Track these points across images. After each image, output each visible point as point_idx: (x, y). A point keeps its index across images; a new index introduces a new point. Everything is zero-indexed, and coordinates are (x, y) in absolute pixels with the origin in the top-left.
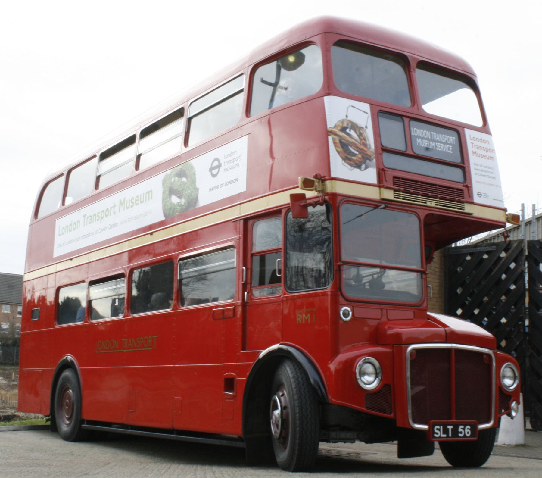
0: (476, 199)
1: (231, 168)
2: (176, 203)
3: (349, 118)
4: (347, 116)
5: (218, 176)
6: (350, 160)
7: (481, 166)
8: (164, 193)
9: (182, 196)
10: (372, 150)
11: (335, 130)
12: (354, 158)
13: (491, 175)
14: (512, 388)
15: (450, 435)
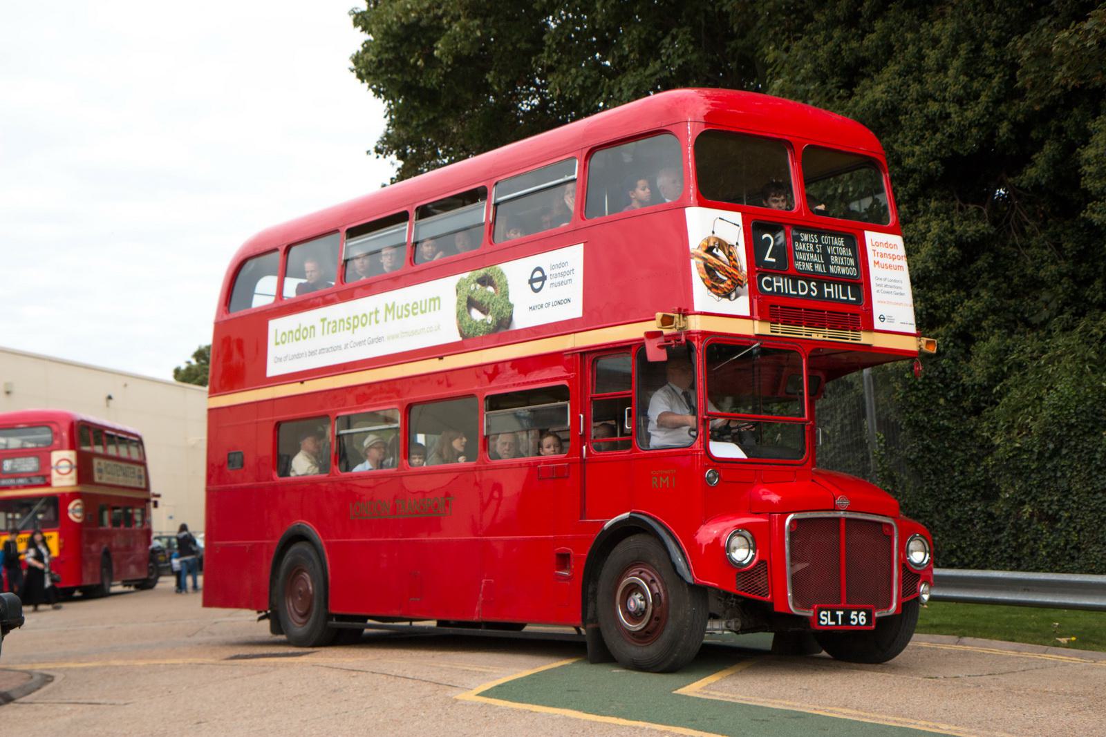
1: (561, 283)
2: (478, 320)
3: (716, 235)
4: (713, 232)
5: (542, 290)
6: (717, 288)
8: (459, 303)
9: (488, 310)
12: (722, 285)
13: (898, 291)
14: (925, 562)
15: (840, 623)
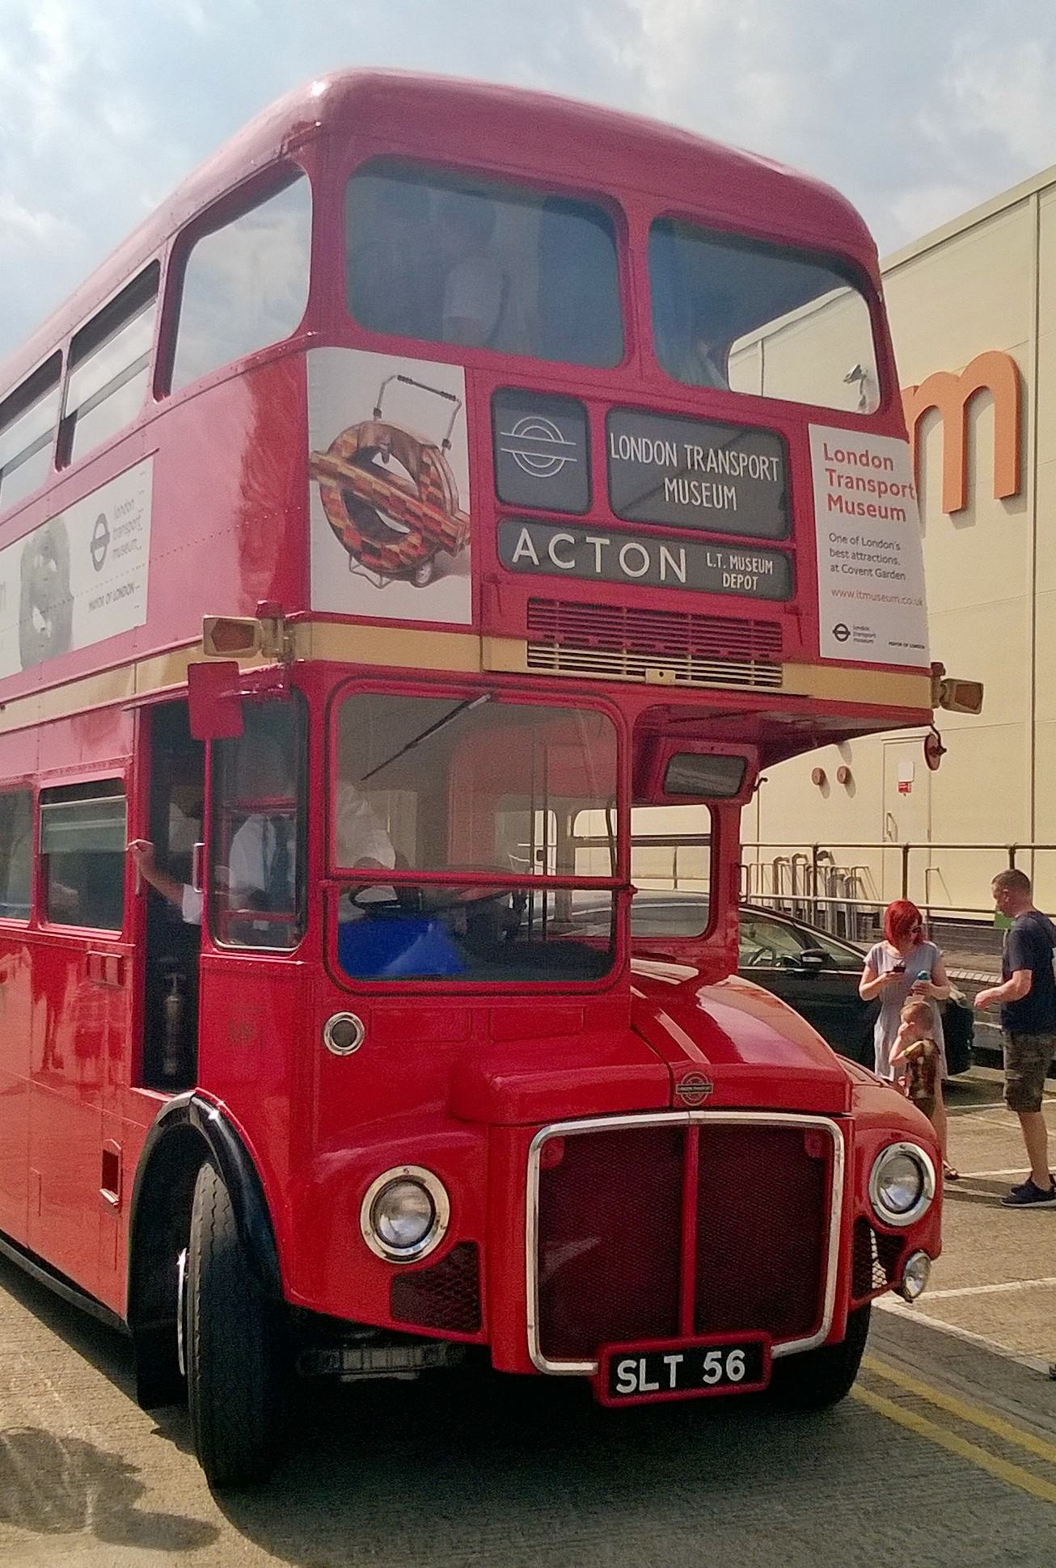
0: (829, 646)
3: (385, 418)
4: (377, 412)
7: (855, 541)
10: (459, 515)
11: (332, 459)
12: (394, 547)
13: (888, 567)
15: (673, 1384)
